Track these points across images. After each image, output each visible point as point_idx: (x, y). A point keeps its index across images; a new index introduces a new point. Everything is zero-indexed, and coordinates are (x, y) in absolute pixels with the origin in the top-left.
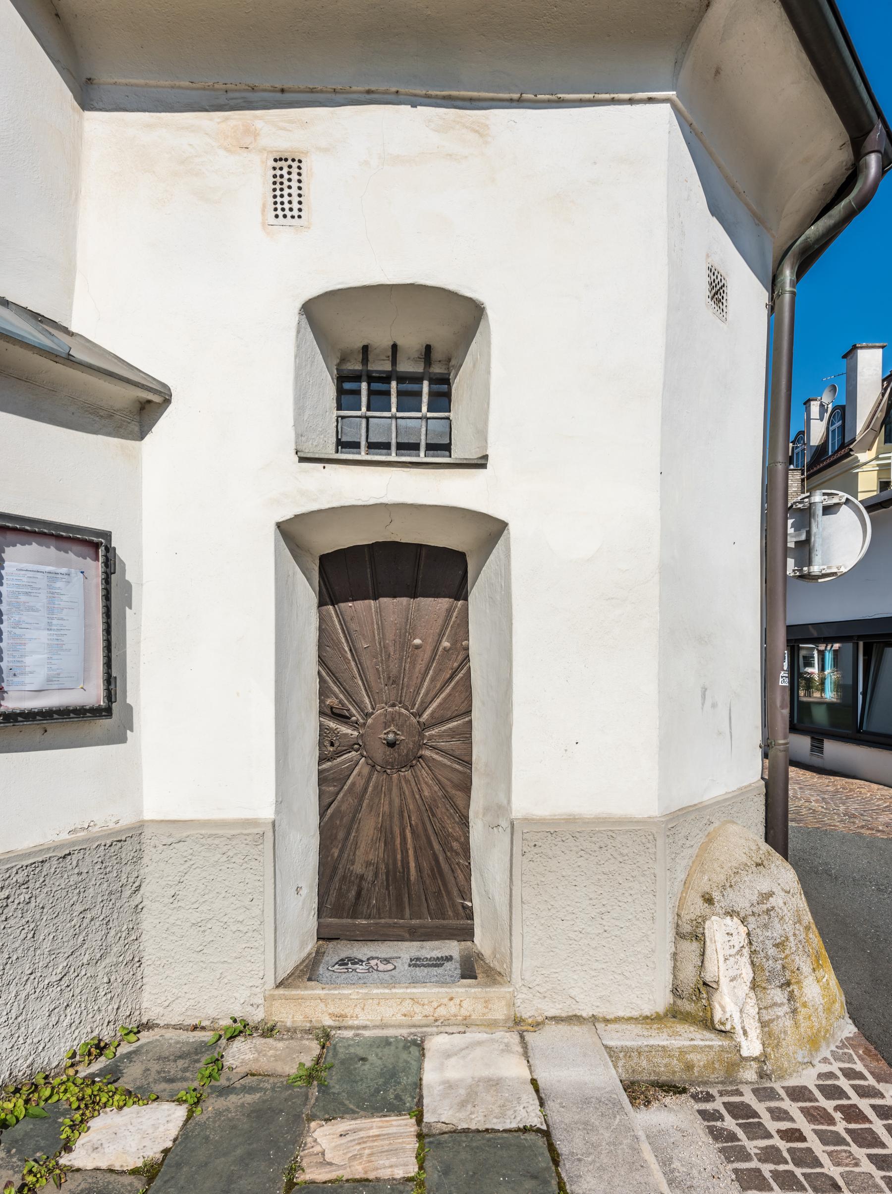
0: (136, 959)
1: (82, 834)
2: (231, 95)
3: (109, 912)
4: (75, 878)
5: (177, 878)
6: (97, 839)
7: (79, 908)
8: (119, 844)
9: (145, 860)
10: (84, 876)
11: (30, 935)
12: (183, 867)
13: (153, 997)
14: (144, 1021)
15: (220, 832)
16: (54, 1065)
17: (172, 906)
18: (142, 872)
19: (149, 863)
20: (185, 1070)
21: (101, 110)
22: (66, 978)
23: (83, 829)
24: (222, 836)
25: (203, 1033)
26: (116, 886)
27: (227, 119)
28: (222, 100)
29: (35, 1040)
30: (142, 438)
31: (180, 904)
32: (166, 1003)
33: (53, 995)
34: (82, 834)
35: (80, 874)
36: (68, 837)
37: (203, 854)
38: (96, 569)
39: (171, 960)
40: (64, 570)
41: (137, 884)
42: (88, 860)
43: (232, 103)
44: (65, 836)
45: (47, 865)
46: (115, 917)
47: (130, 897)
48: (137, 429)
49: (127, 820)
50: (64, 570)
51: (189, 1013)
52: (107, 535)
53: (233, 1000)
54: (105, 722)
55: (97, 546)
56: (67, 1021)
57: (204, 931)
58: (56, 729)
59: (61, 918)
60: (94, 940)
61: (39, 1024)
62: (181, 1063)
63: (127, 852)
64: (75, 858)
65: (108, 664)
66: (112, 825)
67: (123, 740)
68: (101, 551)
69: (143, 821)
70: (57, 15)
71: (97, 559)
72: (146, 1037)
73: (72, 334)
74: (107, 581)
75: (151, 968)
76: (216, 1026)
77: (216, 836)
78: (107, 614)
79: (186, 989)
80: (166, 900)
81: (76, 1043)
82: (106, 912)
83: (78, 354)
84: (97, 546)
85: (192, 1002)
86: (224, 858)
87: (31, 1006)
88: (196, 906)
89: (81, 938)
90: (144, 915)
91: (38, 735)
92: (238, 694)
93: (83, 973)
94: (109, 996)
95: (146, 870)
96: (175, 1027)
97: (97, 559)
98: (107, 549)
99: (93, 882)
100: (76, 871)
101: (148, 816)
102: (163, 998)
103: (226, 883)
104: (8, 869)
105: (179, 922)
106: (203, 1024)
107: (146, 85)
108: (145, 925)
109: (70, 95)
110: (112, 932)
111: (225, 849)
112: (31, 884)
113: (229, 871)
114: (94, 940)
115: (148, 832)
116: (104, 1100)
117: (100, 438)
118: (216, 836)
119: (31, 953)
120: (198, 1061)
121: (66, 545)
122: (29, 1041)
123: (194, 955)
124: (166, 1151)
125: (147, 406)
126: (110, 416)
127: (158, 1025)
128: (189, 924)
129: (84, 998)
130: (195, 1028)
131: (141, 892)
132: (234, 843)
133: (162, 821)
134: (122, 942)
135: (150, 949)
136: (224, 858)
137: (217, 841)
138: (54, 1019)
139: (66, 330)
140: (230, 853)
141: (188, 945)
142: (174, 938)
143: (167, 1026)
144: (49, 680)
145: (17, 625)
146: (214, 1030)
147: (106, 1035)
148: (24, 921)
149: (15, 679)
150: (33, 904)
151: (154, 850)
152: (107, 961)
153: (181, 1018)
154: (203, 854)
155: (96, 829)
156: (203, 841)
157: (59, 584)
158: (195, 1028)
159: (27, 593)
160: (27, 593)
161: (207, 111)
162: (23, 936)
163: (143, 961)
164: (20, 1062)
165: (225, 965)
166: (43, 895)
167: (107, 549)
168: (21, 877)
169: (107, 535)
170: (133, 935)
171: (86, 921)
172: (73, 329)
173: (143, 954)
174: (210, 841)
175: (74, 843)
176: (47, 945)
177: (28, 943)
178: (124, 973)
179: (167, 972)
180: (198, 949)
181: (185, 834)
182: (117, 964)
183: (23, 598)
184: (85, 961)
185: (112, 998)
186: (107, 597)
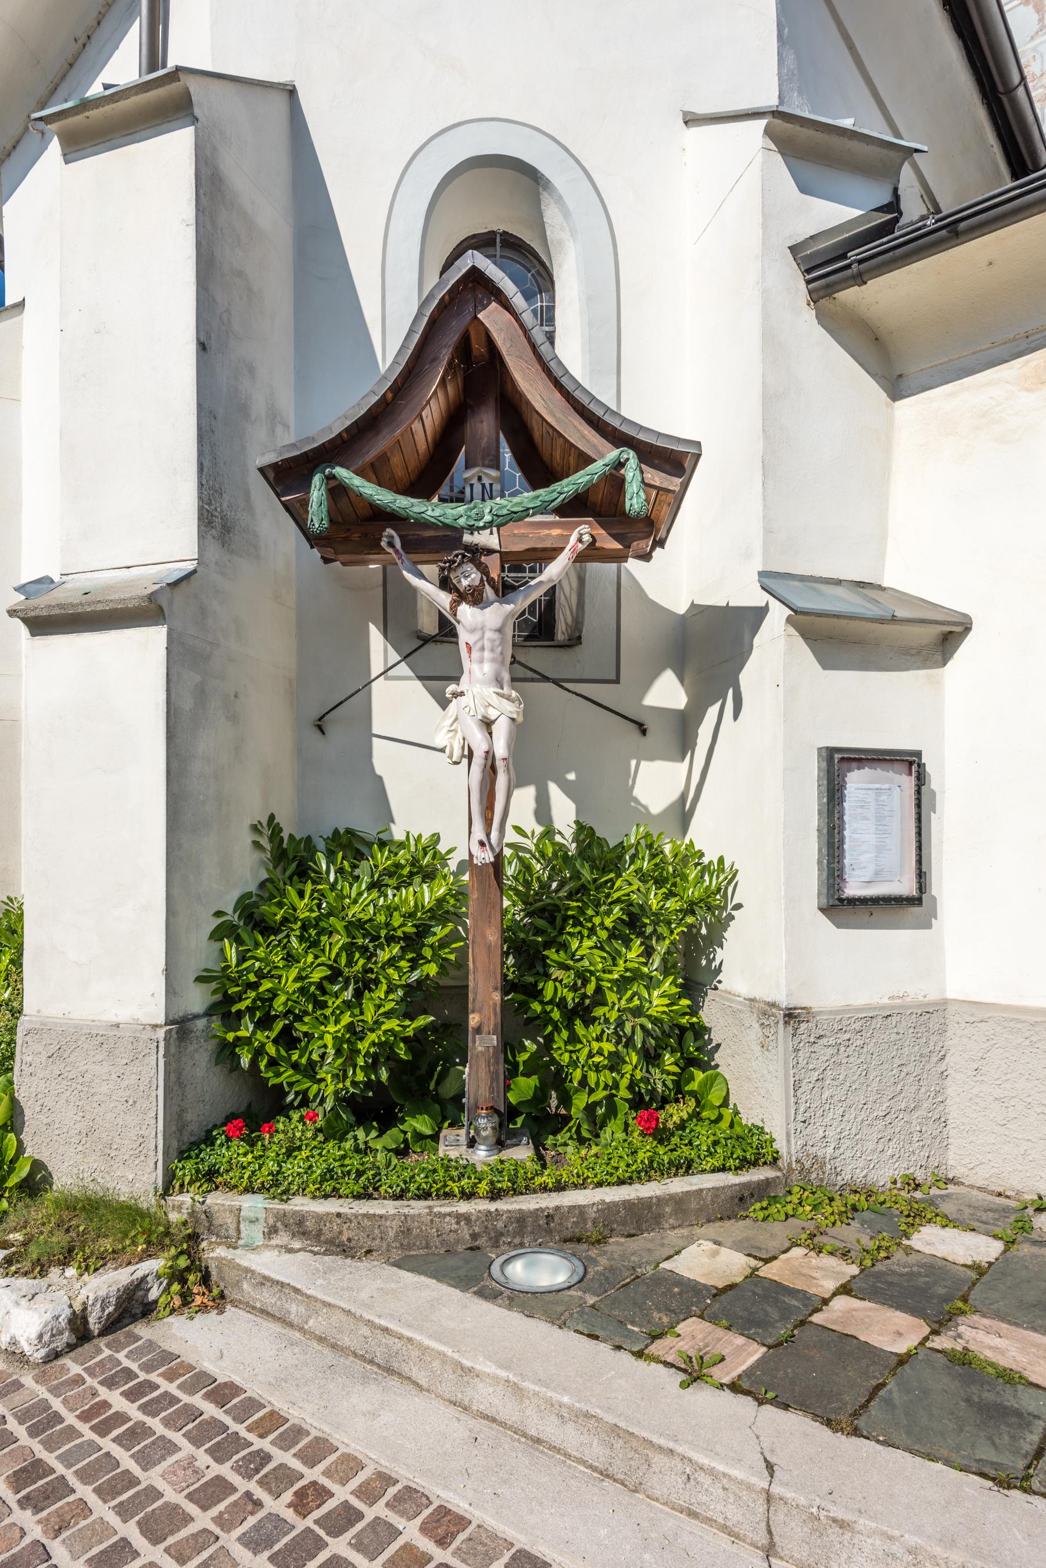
0: (943, 1119)
1: (898, 1001)
2: (1031, 339)
3: (920, 1072)
4: (894, 1036)
5: (980, 1054)
6: (910, 1007)
7: (897, 1061)
8: (928, 1015)
9: (949, 1034)
10: (901, 1036)
11: (864, 1073)
12: (984, 1046)
13: (957, 1157)
14: (950, 1176)
15: (1022, 1017)
16: (881, 1184)
17: (975, 1079)
18: (946, 1043)
19: (953, 1037)
20: (995, 1220)
21: (909, 396)
22: (888, 1116)
23: (899, 997)
24: (1025, 1022)
25: (1007, 1200)
26: (926, 1051)
27: (1028, 362)
28: (1024, 345)
29: (869, 1158)
30: (945, 665)
31: (982, 1078)
32: (971, 1166)
33: (880, 1126)
34: (898, 1001)
35: (897, 1033)
36: (888, 1001)
37: (1005, 1035)
38: (908, 782)
39: (974, 1128)
40: (886, 786)
41: (942, 1053)
42: (904, 1023)
43: (1032, 345)
44: (886, 1001)
45: (874, 1021)
46: (925, 1076)
47: (937, 1063)
48: (940, 658)
49: (933, 996)
50: (886, 786)
51: (993, 1180)
52: (918, 754)
53: (1038, 1178)
54: (915, 910)
55: (911, 763)
56: (890, 1152)
57: (1007, 1107)
58: (878, 912)
59: (885, 1066)
60: (910, 1090)
61: (871, 1146)
62: (990, 1214)
63: (934, 1021)
64: (894, 1019)
65: (919, 861)
66: (921, 998)
67: (928, 926)
68: (914, 768)
69: (945, 1002)
70: (877, 339)
71: (910, 774)
72: (952, 1189)
73: (883, 589)
74: (919, 792)
75: (955, 1131)
76: (1021, 1198)
77: (1018, 1021)
78: (919, 820)
79: (989, 1157)
80: (970, 1073)
81: (896, 1173)
82: (918, 1071)
83: (901, 613)
84: (911, 763)
85: (996, 1170)
86: (1027, 1042)
87: (865, 1130)
88: (998, 1082)
89: (899, 1087)
90: (948, 1082)
91: (866, 917)
92: (1040, 890)
93: (901, 1116)
94: (921, 1143)
95: (950, 1042)
96: (979, 1189)
97: (910, 774)
98: (919, 765)
99: (908, 1043)
100: (895, 1030)
101: (950, 995)
102: (968, 1161)
103: (1030, 1066)
104: (849, 1018)
105: (981, 1095)
106: (1008, 1193)
107: (950, 361)
108: (950, 1091)
109: (885, 394)
110: (923, 1090)
111: (1028, 1034)
112: (863, 1033)
113: (1033, 1055)
114: (910, 1090)
115: (951, 1009)
116: (928, 1216)
117: (911, 672)
118: (1018, 1021)
119: (864, 1087)
120: (1008, 1217)
121: (875, 764)
122: (864, 1157)
123: (998, 1127)
124: (990, 1264)
125: (949, 637)
126: (919, 653)
127: (963, 1184)
128: (992, 1098)
129: (902, 1137)
130: (1000, 1195)
131: (946, 1060)
132: (1037, 1029)
133: (964, 1001)
134: (930, 1100)
135: (954, 1114)
136: (1027, 1042)
137: (1019, 1026)
138: (880, 1147)
139: (880, 588)
140: (1034, 1039)
141: (991, 1117)
142: (977, 1108)
143: (972, 1187)
144: (877, 873)
145: (854, 832)
146: (1019, 1201)
147: (920, 1176)
148: (860, 1061)
149: (854, 873)
150: (865, 1050)
151: (957, 1026)
152: (919, 1113)
153: (986, 1183)
154: (1005, 1035)
155: (908, 999)
156: (1005, 1024)
157: (883, 798)
158: (1000, 1195)
159: (861, 807)
160: (861, 807)
161: (1007, 361)
162: (859, 1072)
163: (948, 1122)
164: (858, 1171)
165: (1030, 1144)
166: (872, 1044)
167: (919, 765)
168: (857, 1026)
169: (918, 754)
170: (939, 1097)
171: (903, 1074)
172: (885, 585)
173: (949, 1117)
174: (1012, 1024)
175: (893, 1007)
176: (875, 1084)
177: (862, 1080)
178: (931, 1128)
179: (972, 1138)
180: (1002, 1123)
181: (987, 1016)
182: (927, 1118)
183: (859, 810)
184: (903, 1107)
185: (923, 1146)
186: (919, 805)
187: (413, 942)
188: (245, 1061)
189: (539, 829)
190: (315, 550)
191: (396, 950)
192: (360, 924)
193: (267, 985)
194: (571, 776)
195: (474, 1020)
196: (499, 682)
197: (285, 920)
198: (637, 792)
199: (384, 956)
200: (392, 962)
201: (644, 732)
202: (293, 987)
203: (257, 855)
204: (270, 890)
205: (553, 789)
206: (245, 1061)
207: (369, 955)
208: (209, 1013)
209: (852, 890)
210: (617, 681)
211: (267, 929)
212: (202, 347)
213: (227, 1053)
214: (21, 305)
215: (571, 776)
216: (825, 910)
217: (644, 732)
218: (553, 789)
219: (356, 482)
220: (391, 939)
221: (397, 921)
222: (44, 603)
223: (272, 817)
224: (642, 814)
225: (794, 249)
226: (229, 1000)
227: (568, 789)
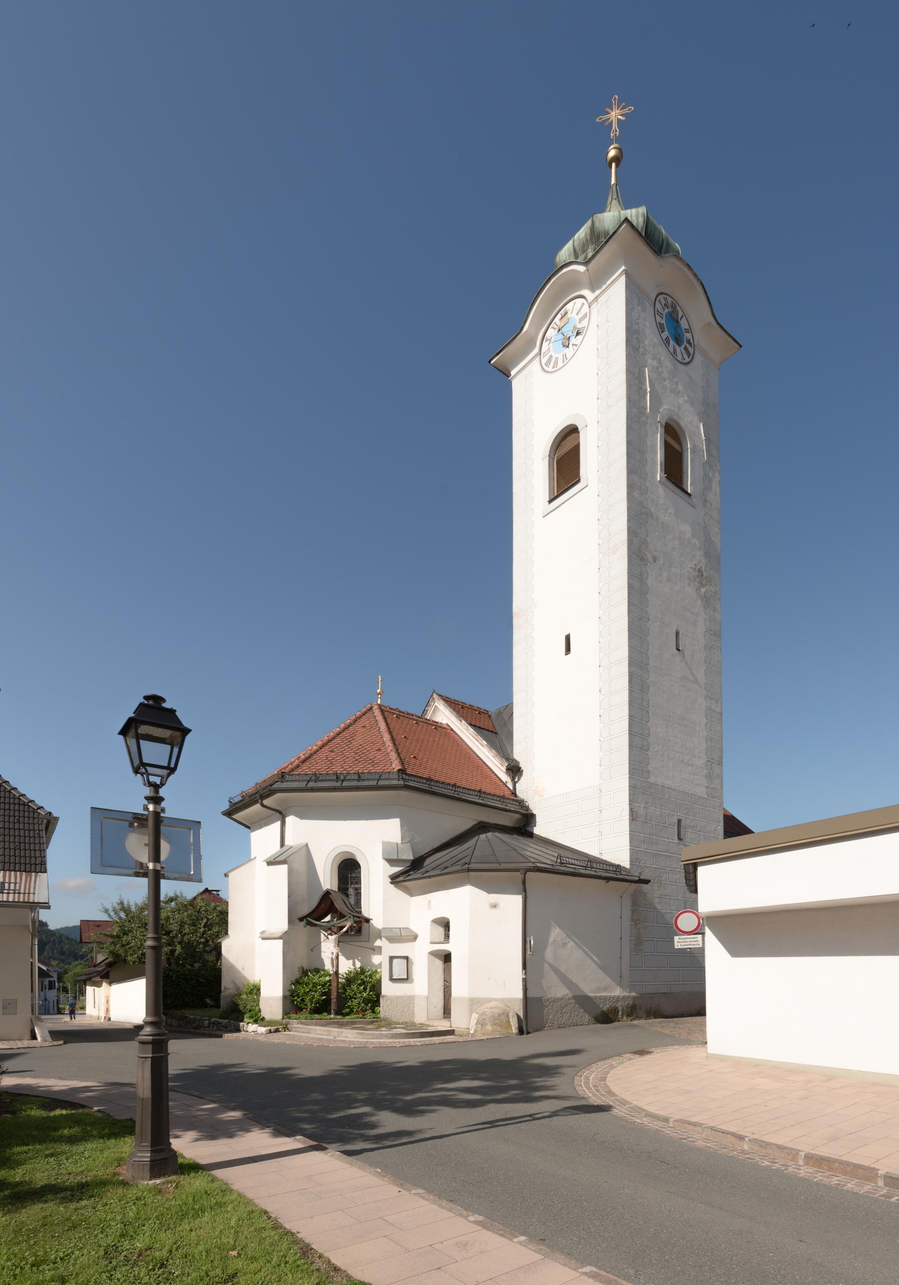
38: (406, 961)
69: (414, 996)
187: (323, 986)
188: (295, 1003)
189: (354, 968)
190: (445, 723)
191: (320, 987)
192: (315, 983)
193: (298, 991)
194: (360, 958)
195: (332, 997)
196: (335, 947)
197: (303, 982)
198: (373, 961)
199: (318, 988)
200: (320, 989)
201: (374, 950)
202: (303, 992)
203: (299, 972)
204: (301, 977)
205: (356, 960)
206: (295, 1003)
207: (316, 987)
208: (290, 996)
209: (394, 977)
210: (369, 941)
211: (300, 984)
212: (289, 897)
213: (293, 1002)
214: (255, 858)
215: (360, 958)
216: (390, 980)
217: (374, 950)
218: (356, 960)
219: (311, 920)
220: (320, 985)
221: (321, 982)
222: (264, 935)
223: (302, 966)
224: (374, 965)
225: (389, 876)
226: (293, 994)
227: (358, 960)
